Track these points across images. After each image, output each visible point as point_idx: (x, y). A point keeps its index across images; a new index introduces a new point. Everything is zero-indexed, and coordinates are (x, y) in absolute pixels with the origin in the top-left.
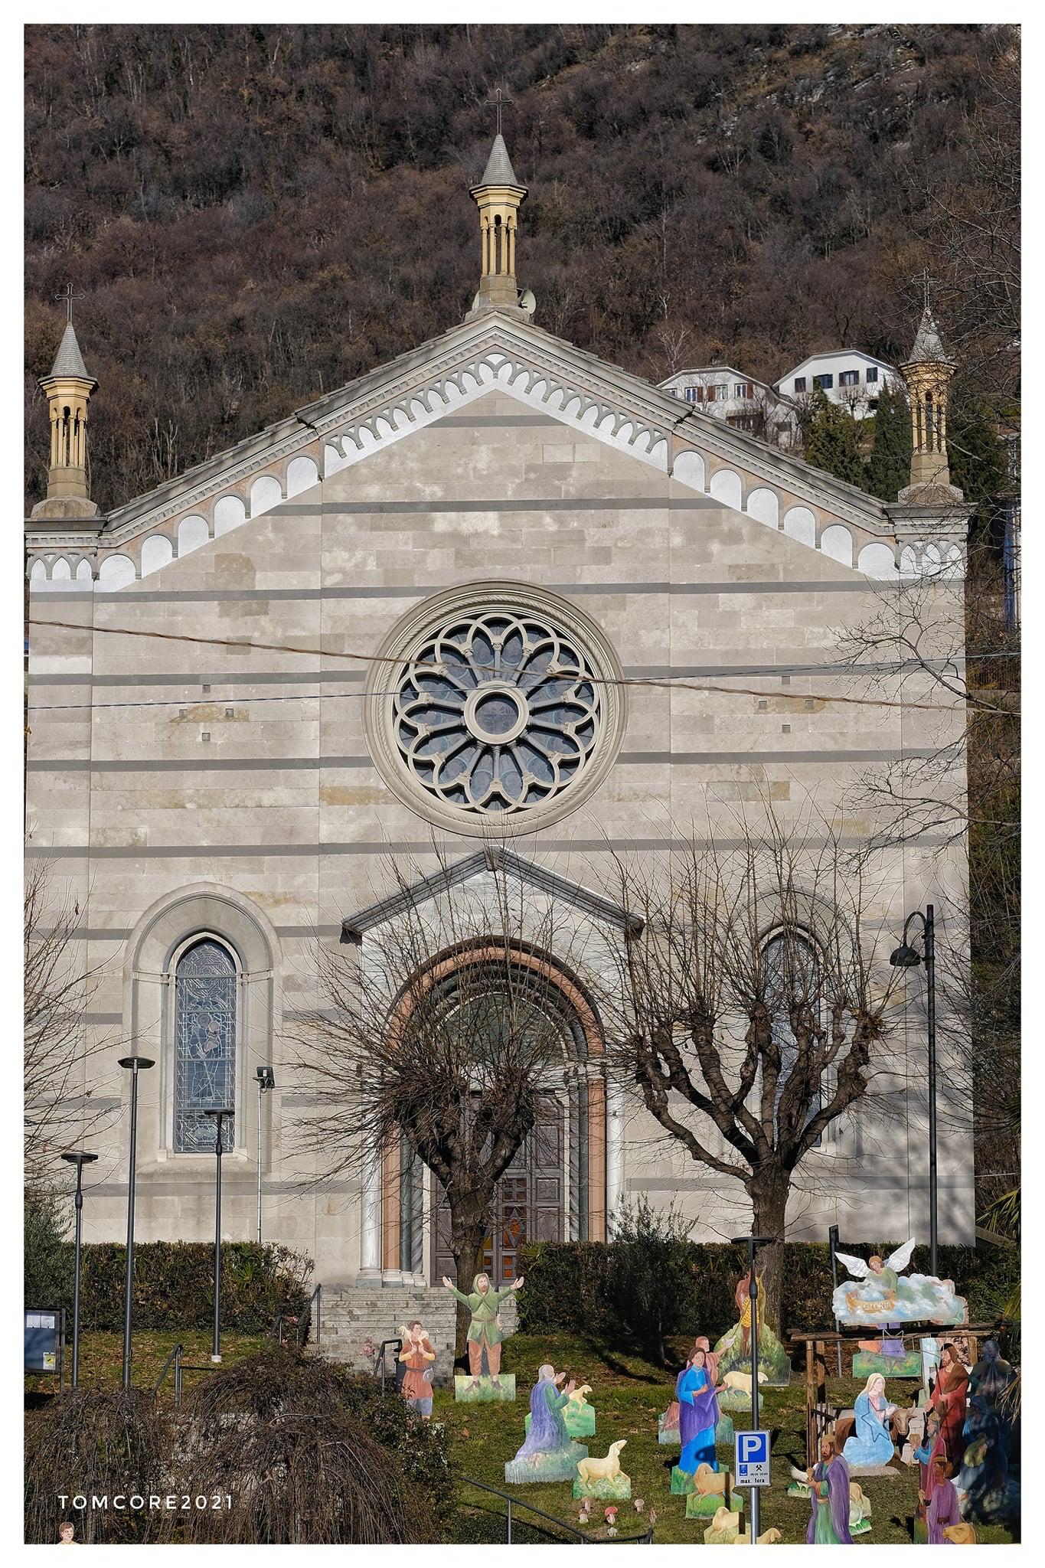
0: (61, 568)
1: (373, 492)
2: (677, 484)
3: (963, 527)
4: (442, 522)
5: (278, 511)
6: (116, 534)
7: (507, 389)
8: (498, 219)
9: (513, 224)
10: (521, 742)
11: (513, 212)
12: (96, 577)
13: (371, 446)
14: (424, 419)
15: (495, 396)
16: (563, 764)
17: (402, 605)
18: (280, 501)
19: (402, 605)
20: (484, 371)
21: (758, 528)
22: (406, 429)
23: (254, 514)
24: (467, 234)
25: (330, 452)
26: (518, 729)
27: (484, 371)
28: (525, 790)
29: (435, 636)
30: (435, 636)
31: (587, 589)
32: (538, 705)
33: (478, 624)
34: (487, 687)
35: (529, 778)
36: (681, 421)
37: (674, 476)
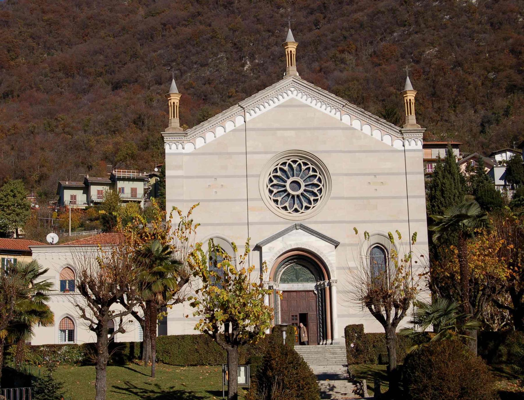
0: (174, 146)
1: (259, 126)
2: (343, 123)
3: (421, 135)
4: (279, 133)
5: (233, 131)
6: (189, 137)
7: (295, 97)
8: (174, 103)
9: (178, 105)
10: (298, 196)
11: (295, 50)
12: (183, 148)
13: (259, 113)
14: (273, 105)
15: (293, 99)
16: (314, 200)
17: (269, 156)
18: (234, 128)
19: (269, 156)
20: (289, 92)
21: (366, 135)
22: (268, 108)
23: (227, 132)
24: (283, 55)
25: (247, 115)
26: (299, 193)
27: (289, 92)
28: (294, 209)
29: (277, 165)
30: (277, 165)
31: (322, 152)
32: (307, 184)
33: (289, 162)
34: (295, 179)
35: (296, 206)
36: (344, 106)
37: (343, 121)
